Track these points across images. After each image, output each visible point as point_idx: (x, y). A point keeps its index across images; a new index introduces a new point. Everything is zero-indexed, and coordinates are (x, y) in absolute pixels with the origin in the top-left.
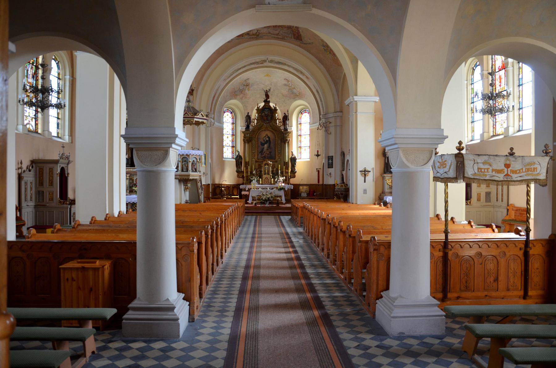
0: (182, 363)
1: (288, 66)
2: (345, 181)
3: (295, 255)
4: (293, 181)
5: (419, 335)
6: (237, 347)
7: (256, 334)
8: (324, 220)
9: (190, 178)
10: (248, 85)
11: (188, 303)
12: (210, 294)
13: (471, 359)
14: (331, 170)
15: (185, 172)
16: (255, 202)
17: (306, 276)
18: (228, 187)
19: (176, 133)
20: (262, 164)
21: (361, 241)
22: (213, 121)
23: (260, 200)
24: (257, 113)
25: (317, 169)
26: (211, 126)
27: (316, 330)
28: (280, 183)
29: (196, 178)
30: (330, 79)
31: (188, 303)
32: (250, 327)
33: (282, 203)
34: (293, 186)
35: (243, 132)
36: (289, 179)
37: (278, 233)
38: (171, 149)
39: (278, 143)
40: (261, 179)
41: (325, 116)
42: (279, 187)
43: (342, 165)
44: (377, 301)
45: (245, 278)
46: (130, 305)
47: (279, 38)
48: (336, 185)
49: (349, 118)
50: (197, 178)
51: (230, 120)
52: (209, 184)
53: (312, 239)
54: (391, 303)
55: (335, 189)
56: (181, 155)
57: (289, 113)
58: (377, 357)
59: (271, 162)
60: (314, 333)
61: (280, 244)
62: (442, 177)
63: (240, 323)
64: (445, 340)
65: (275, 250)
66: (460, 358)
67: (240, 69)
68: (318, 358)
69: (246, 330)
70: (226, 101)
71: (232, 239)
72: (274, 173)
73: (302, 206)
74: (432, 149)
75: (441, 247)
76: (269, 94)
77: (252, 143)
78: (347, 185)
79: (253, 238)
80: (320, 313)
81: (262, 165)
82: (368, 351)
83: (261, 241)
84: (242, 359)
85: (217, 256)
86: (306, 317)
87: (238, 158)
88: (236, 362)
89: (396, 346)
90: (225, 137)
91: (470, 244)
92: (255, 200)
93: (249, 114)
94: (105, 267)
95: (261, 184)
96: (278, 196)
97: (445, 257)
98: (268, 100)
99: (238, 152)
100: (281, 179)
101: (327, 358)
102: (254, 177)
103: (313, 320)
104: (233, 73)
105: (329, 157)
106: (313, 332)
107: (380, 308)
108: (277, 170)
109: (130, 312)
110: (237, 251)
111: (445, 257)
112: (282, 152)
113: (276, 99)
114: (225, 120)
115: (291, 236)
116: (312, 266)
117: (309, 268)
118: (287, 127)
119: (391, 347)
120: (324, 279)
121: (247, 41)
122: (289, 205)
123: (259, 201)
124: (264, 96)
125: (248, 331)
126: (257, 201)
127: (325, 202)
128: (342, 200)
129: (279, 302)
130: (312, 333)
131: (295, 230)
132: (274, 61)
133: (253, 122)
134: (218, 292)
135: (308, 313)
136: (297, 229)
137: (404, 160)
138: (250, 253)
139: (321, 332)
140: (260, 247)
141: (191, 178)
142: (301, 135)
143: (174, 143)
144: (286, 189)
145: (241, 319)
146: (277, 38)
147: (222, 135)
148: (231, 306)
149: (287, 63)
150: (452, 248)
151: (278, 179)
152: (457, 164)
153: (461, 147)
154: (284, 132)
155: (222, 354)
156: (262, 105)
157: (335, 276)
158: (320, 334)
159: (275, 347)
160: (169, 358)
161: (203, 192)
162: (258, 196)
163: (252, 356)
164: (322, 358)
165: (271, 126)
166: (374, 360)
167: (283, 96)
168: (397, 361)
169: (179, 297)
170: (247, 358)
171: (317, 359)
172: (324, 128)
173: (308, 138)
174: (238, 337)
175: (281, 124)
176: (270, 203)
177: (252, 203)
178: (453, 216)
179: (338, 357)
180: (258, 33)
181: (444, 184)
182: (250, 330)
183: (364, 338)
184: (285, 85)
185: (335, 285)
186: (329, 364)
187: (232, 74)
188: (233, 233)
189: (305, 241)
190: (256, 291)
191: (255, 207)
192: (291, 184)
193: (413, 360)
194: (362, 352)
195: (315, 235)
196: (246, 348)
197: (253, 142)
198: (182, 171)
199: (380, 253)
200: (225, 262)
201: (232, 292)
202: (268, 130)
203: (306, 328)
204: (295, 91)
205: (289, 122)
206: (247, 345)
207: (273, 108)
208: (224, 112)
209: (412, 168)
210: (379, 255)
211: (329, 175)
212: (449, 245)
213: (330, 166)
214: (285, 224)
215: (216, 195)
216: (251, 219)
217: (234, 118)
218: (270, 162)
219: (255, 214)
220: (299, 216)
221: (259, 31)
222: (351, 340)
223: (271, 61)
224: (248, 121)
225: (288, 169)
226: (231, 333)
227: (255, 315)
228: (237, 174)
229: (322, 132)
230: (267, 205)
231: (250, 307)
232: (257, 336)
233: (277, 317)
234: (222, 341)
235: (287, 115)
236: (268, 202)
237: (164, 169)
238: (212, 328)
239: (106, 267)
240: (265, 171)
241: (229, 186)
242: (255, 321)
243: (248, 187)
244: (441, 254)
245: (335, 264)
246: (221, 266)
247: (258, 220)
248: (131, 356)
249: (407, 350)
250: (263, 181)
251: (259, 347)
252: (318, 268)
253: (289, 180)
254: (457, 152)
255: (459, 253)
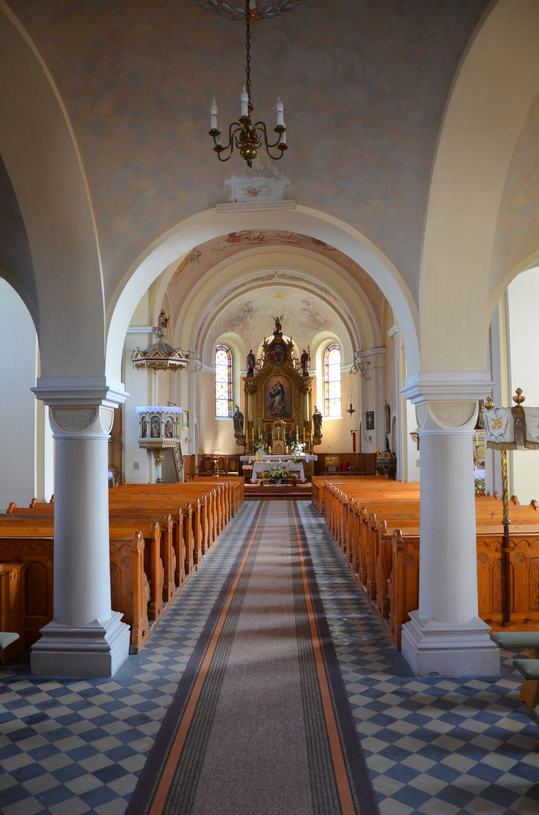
0: (106, 712)
1: (307, 282)
2: (391, 448)
3: (305, 558)
4: (317, 449)
5: (460, 677)
6: (190, 691)
7: (221, 673)
8: (345, 505)
9: (163, 446)
10: (250, 311)
11: (129, 627)
12: (168, 615)
13: (531, 713)
14: (371, 433)
15: (156, 437)
16: (260, 480)
17: (315, 589)
18: (222, 459)
19: (107, 385)
20: (272, 425)
21: (384, 536)
22: (200, 363)
23: (268, 477)
24: (264, 350)
25: (352, 431)
26: (196, 371)
27: (309, 668)
28: (298, 452)
29: (171, 446)
30: (367, 299)
31: (129, 627)
32: (216, 662)
33: (301, 482)
34: (317, 456)
35: (244, 379)
36: (312, 447)
37: (287, 526)
38: (100, 407)
39: (294, 394)
40: (270, 447)
41: (361, 354)
42: (295, 458)
43: (387, 425)
44: (403, 625)
45: (224, 592)
46: (43, 629)
47: (292, 243)
48: (378, 454)
49: (394, 356)
50: (173, 446)
51: (226, 362)
52: (194, 455)
53: (334, 535)
54: (419, 627)
55: (376, 460)
56: (149, 413)
57: (311, 349)
58: (392, 708)
59: (284, 421)
60: (307, 672)
61: (287, 542)
62: (497, 441)
63: (203, 656)
64: (498, 684)
65: (277, 550)
66: (515, 711)
67: (238, 287)
68: (303, 708)
69: (208, 666)
70: (219, 335)
71: (218, 534)
72: (290, 438)
73: (324, 485)
74: (474, 402)
75: (499, 545)
76: (281, 323)
77: (257, 395)
78: (394, 454)
79: (250, 533)
80: (321, 643)
81: (272, 426)
82: (380, 699)
83: (260, 538)
84: (193, 708)
85: (187, 560)
86: (300, 649)
87: (238, 416)
88: (184, 713)
89: (422, 692)
90: (218, 387)
91: (515, 541)
92: (261, 478)
93: (253, 353)
94: (10, 574)
95: (271, 454)
96: (294, 472)
97: (505, 561)
98: (280, 332)
99: (237, 407)
100: (300, 446)
101: (316, 708)
102: (260, 444)
103: (309, 652)
104: (228, 293)
105: (369, 414)
106: (305, 670)
107: (406, 636)
108: (294, 433)
109: (42, 639)
110: (223, 551)
111: (505, 561)
112: (301, 406)
113: (291, 331)
114: (218, 361)
115: (306, 530)
116: (328, 573)
117: (322, 576)
118: (307, 370)
119: (415, 693)
120: (339, 593)
121: (247, 249)
122: (309, 485)
123: (266, 479)
124: (275, 326)
125: (211, 668)
126: (264, 479)
127: (361, 479)
128: (387, 476)
129: (266, 627)
130: (303, 671)
131: (313, 521)
132: (287, 275)
133: (258, 364)
134: (181, 612)
135: (302, 643)
136: (317, 519)
137: (434, 418)
138: (240, 555)
139: (316, 670)
140: (257, 546)
141: (164, 446)
142: (328, 382)
143: (104, 398)
144: (307, 461)
145: (205, 651)
146: (289, 242)
147: (213, 383)
148: (195, 632)
149: (305, 279)
150: (515, 545)
151: (295, 447)
152: (515, 422)
153: (520, 397)
154: (304, 378)
155: (166, 701)
156: (271, 339)
157: (357, 589)
158: (315, 673)
159: (244, 691)
160: (90, 705)
161: (183, 466)
162: (265, 471)
163: (209, 704)
164: (309, 708)
165: (284, 370)
166: (384, 712)
167: (302, 325)
168: (418, 714)
169: (113, 619)
170: (201, 707)
171: (302, 709)
172: (359, 372)
173: (338, 386)
174: (195, 677)
175: (300, 366)
176: (283, 482)
177: (256, 483)
178: (533, 499)
179: (333, 707)
180: (261, 237)
181: (500, 451)
182: (215, 667)
183: (377, 680)
184: (304, 309)
185: (354, 602)
186: (318, 717)
187: (227, 296)
188: (220, 525)
189: (325, 537)
190: (235, 611)
191: (261, 489)
192: (314, 454)
193: (442, 713)
194: (370, 700)
195: (337, 528)
196: (203, 692)
197: (259, 393)
198: (152, 436)
199: (407, 555)
200: (201, 568)
201: (201, 612)
202: (280, 375)
203: (296, 665)
204: (318, 317)
205: (310, 364)
206: (205, 688)
207: (287, 343)
208: (217, 351)
209: (446, 428)
210: (407, 557)
211: (368, 439)
212: (510, 542)
213: (370, 426)
214: (301, 512)
215: (205, 470)
216: (253, 504)
217: (232, 359)
218: (283, 422)
219: (260, 498)
220: (321, 500)
221: (263, 234)
222: (358, 682)
223: (283, 276)
224: (252, 363)
225: (310, 432)
226: (186, 671)
227: (227, 645)
228: (236, 440)
229: (357, 377)
230: (278, 485)
231: (222, 634)
232: (222, 676)
233: (258, 648)
234: (171, 682)
235: (307, 352)
236: (280, 481)
237: (90, 435)
238: (160, 663)
239: (12, 574)
240: (276, 435)
241: (224, 457)
242: (225, 654)
243: (251, 458)
244: (499, 555)
245: (357, 571)
246: (193, 573)
247: (262, 507)
248: (36, 702)
249: (437, 698)
250: (274, 450)
251: (221, 691)
252: (334, 577)
253: (311, 448)
254: (514, 404)
255: (525, 554)
